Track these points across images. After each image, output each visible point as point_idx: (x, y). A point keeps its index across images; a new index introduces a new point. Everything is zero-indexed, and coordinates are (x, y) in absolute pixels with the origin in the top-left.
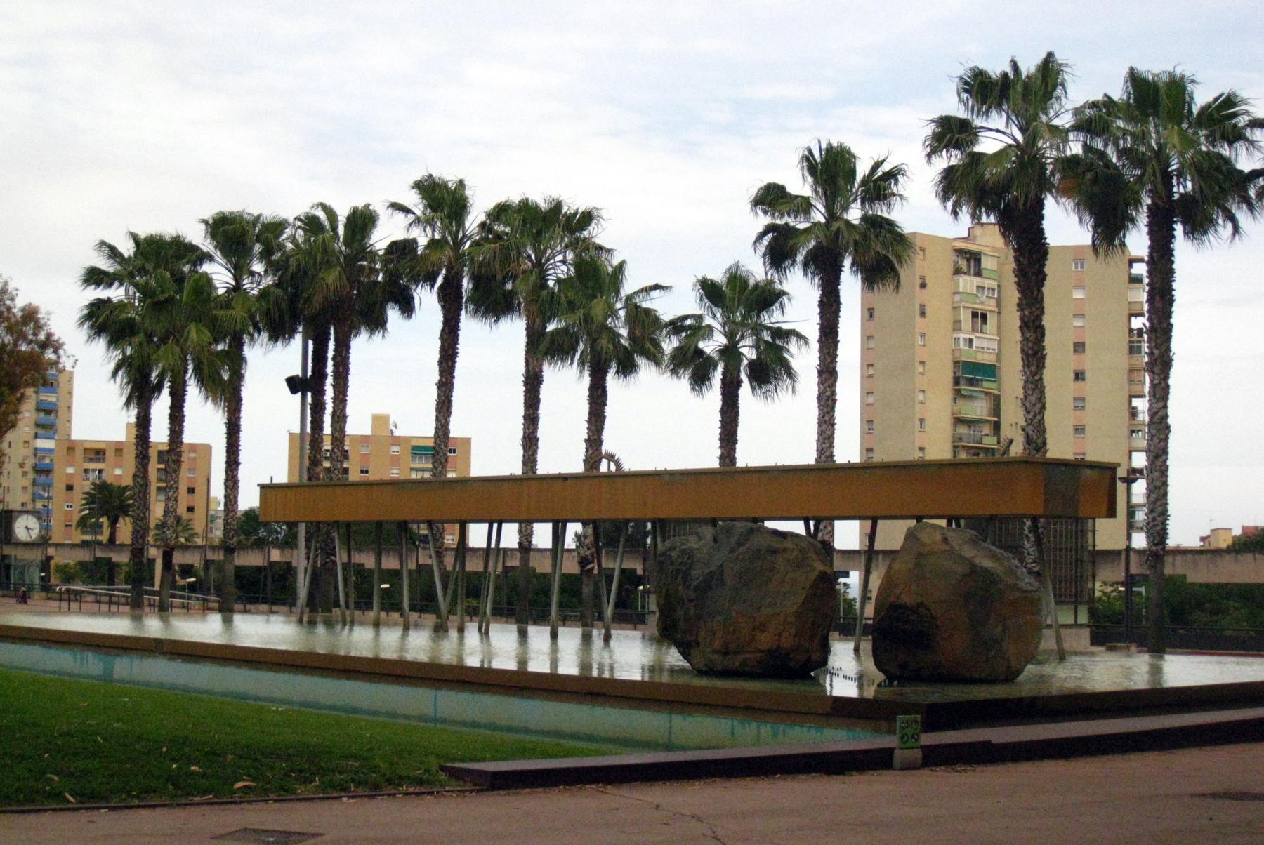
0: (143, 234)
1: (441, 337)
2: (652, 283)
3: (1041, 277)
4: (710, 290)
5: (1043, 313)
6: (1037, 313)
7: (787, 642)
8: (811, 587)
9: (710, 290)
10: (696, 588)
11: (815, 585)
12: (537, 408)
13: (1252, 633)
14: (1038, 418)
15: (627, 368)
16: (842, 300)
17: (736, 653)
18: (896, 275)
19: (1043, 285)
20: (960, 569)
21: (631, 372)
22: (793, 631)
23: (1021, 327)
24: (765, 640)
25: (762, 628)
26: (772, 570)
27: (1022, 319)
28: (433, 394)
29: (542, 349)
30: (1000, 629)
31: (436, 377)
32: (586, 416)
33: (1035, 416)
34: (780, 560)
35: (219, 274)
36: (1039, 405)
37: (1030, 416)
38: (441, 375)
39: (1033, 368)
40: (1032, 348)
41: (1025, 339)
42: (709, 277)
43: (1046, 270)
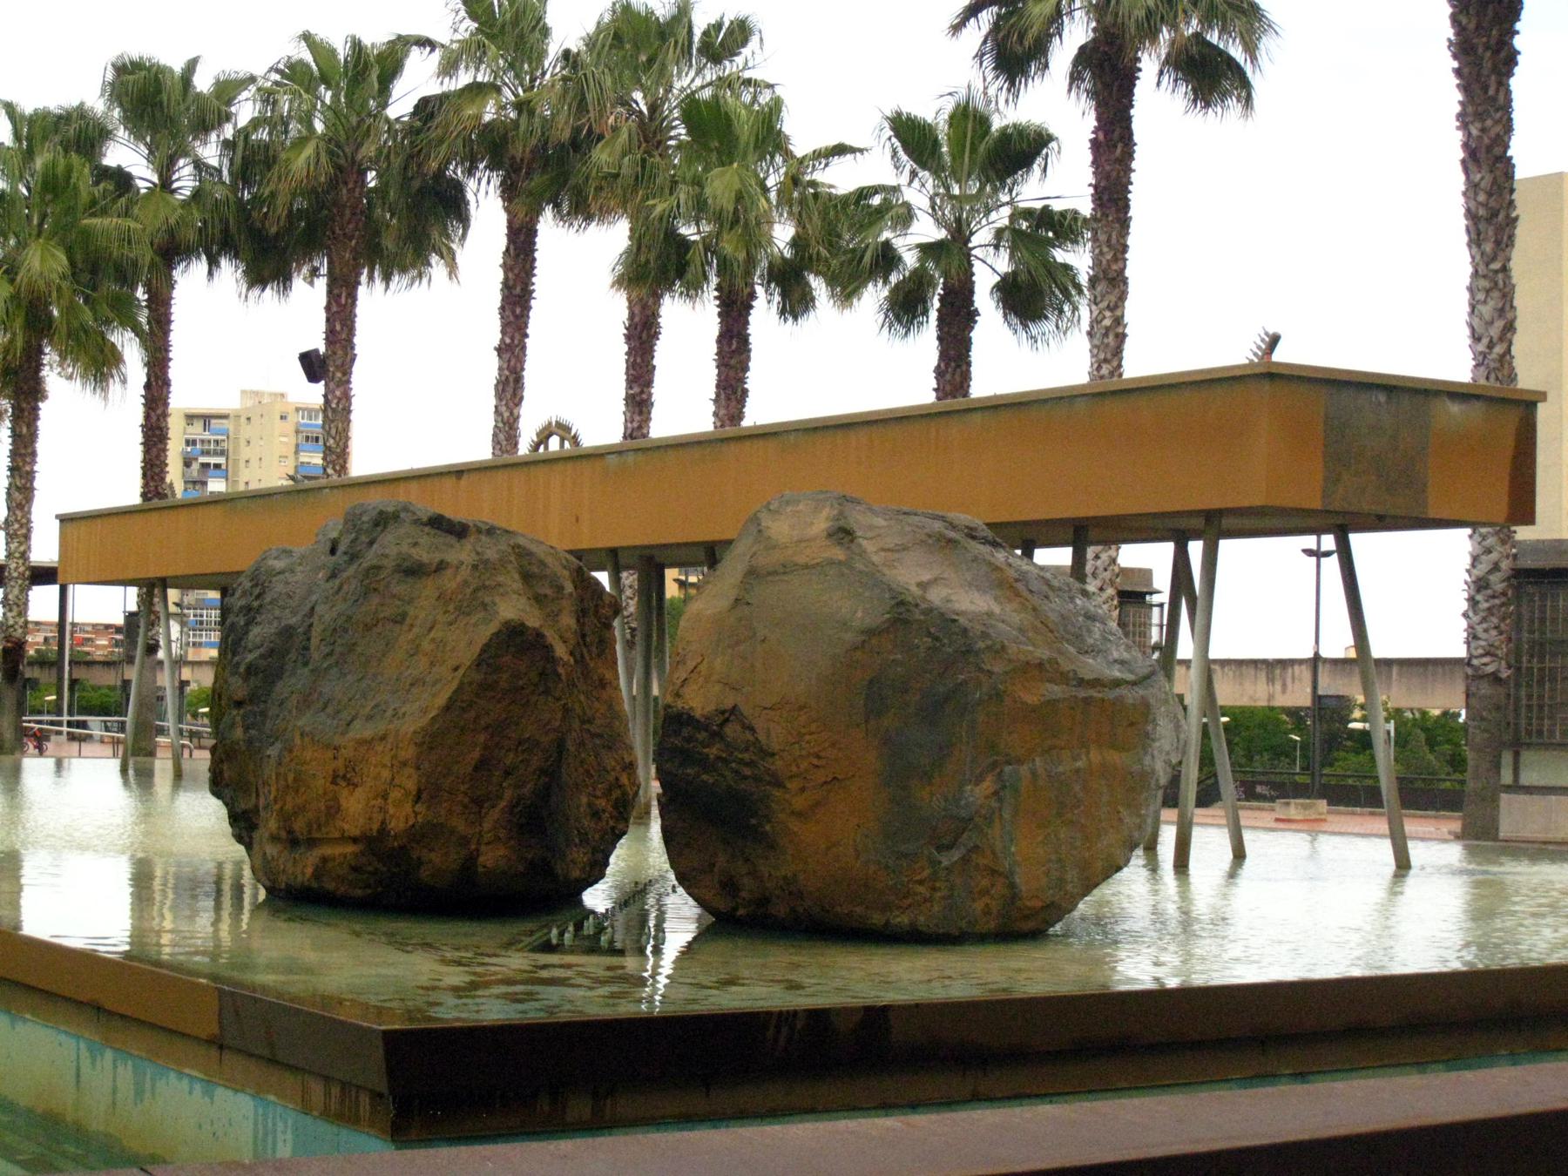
0: (27, 107)
1: (505, 266)
2: (832, 142)
3: (1508, 60)
4: (912, 137)
5: (1509, 129)
6: (1498, 129)
7: (401, 816)
8: (478, 664)
9: (912, 137)
10: (251, 670)
11: (488, 658)
12: (649, 383)
13: (753, 821)
14: (1499, 349)
15: (796, 304)
16: (1136, 138)
17: (312, 843)
18: (1245, 84)
19: (1510, 74)
20: (862, 612)
21: (806, 310)
22: (411, 785)
23: (1463, 162)
24: (356, 808)
25: (345, 777)
26: (400, 619)
27: (1465, 146)
28: (491, 367)
29: (654, 272)
30: (988, 785)
31: (495, 336)
32: (711, 391)
33: (1491, 346)
34: (427, 590)
35: (126, 154)
36: (1500, 324)
37: (1481, 347)
38: (503, 332)
39: (1488, 247)
40: (1485, 205)
41: (1472, 189)
42: (905, 110)
43: (1518, 42)
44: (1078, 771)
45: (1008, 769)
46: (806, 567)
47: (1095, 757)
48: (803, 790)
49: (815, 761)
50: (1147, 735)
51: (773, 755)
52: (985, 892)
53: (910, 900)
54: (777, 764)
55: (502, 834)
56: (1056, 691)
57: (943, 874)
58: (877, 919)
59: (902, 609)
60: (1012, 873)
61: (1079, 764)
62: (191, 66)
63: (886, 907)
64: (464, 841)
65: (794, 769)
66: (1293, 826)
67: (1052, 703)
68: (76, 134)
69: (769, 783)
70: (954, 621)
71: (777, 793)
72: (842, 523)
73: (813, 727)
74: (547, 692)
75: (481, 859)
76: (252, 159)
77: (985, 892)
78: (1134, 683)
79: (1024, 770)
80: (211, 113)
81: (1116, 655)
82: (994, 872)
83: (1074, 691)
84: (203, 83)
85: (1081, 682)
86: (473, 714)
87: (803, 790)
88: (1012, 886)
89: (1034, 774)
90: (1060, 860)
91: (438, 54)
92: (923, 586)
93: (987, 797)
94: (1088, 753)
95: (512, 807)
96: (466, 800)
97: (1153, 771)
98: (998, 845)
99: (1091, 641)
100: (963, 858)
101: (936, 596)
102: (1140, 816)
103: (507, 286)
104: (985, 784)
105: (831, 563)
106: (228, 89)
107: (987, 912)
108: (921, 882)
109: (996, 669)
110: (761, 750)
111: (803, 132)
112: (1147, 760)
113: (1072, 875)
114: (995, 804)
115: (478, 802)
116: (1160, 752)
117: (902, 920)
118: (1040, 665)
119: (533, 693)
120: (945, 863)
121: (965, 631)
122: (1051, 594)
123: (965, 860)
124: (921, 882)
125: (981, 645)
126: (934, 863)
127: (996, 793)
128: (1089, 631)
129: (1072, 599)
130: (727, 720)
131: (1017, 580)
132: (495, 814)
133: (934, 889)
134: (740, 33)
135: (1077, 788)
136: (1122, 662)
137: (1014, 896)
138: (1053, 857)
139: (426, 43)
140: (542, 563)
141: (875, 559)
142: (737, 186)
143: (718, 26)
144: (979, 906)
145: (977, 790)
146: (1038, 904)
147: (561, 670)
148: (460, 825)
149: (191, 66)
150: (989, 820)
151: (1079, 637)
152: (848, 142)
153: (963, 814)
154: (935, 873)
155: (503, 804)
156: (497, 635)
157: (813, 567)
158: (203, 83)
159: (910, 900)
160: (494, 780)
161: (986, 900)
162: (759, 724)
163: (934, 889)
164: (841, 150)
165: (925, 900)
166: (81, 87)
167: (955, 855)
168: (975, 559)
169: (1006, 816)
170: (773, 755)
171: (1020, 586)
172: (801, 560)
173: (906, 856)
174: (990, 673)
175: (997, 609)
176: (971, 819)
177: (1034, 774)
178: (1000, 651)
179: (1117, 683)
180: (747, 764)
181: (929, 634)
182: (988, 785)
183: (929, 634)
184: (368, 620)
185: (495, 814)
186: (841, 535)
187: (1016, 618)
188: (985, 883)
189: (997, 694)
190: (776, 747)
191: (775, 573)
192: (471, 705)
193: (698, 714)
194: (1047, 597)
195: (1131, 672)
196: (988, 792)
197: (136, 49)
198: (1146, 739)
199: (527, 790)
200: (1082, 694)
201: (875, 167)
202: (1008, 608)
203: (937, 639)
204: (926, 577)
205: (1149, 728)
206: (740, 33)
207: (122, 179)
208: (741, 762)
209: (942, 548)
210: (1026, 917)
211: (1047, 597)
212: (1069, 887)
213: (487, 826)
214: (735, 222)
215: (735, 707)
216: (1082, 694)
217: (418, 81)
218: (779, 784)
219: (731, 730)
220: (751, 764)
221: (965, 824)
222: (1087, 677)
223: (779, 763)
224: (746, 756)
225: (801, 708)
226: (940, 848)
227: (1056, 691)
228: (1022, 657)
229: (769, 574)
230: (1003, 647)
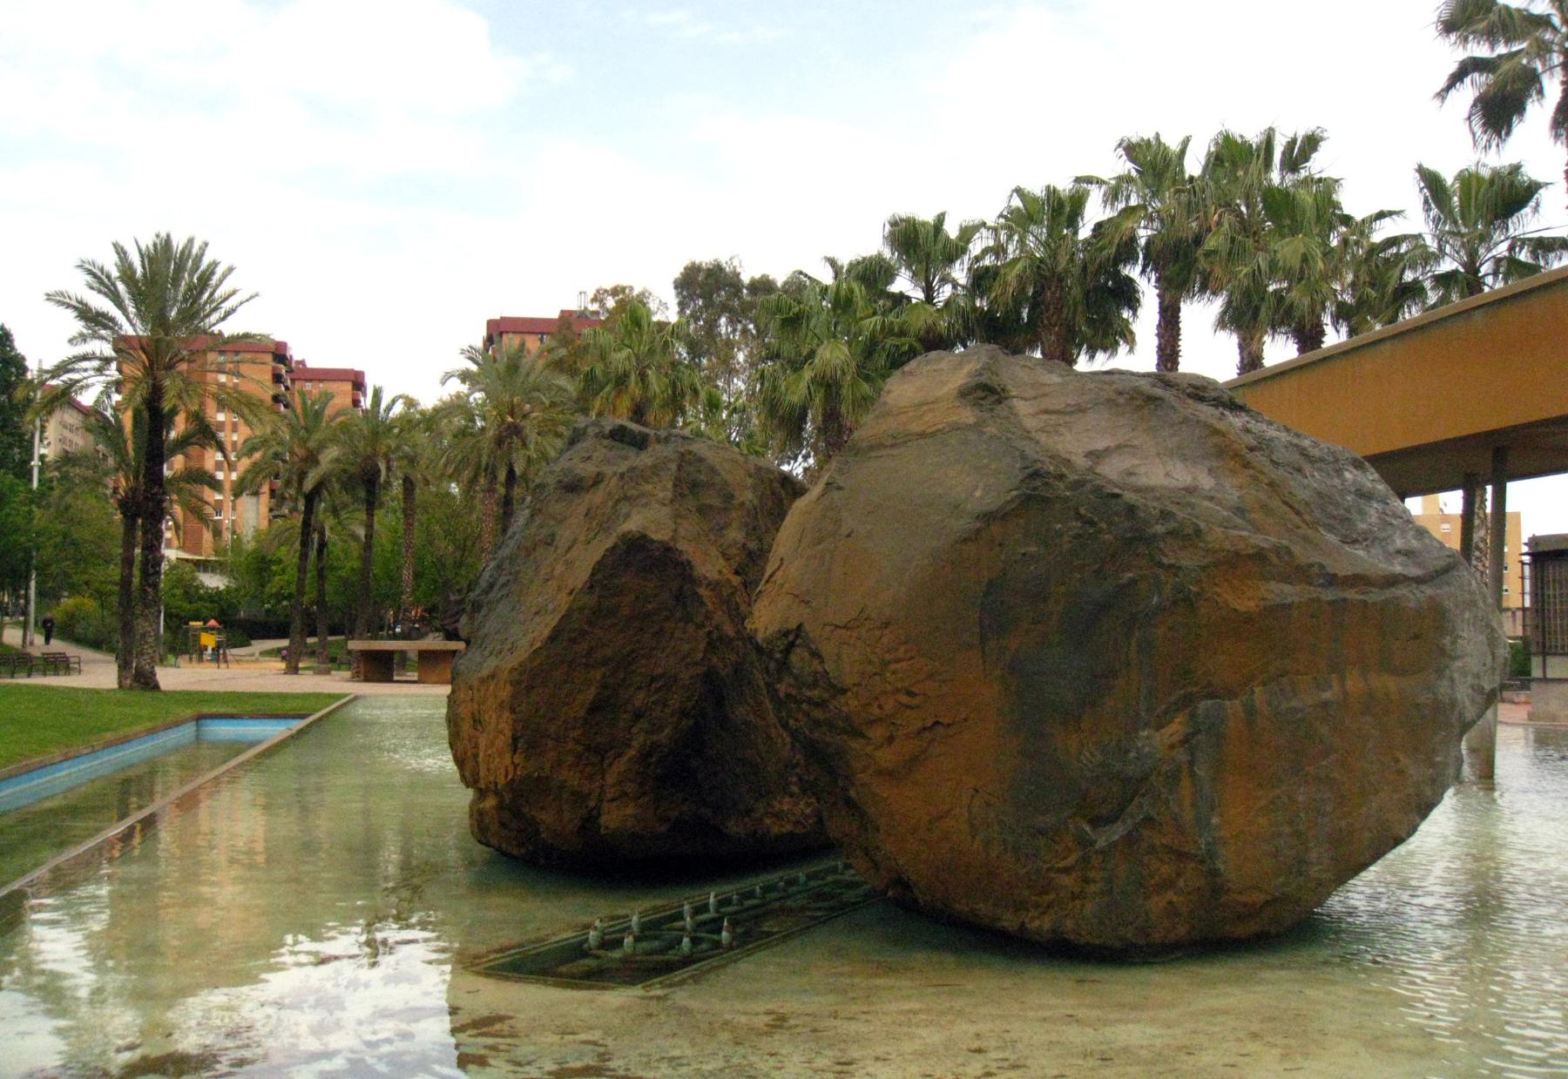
1: (1158, 335)
8: (591, 586)
11: (604, 576)
30: (1177, 728)
44: (1325, 705)
45: (1204, 705)
46: (922, 435)
47: (1354, 683)
48: (891, 739)
49: (904, 699)
50: (1442, 652)
51: (844, 691)
52: (1169, 884)
53: (1052, 896)
54: (850, 704)
55: (631, 788)
56: (1290, 592)
57: (1096, 860)
58: (1008, 921)
59: (1038, 483)
60: (1212, 855)
61: (1327, 695)
62: (941, 219)
63: (1020, 906)
64: (579, 797)
65: (876, 711)
66: (679, 975)
67: (1281, 610)
68: (872, 274)
69: (844, 731)
70: (1117, 496)
71: (856, 744)
72: (984, 379)
73: (901, 653)
74: (687, 619)
75: (603, 819)
76: (981, 279)
77: (1169, 884)
78: (1419, 581)
79: (1233, 707)
80: (954, 252)
81: (1399, 543)
82: (1181, 856)
83: (1313, 592)
84: (952, 230)
85: (1332, 580)
86: (585, 646)
87: (891, 739)
88: (1214, 873)
89: (1251, 711)
90: (1297, 834)
91: (1104, 188)
92: (1093, 455)
93: (1172, 747)
94: (1342, 679)
95: (644, 756)
96: (580, 748)
97: (1453, 703)
98: (1188, 815)
99: (1362, 526)
100: (1129, 834)
101: (1111, 469)
102: (1434, 765)
103: (1161, 349)
104: (1174, 727)
105: (956, 428)
106: (968, 233)
107: (1172, 911)
108: (1066, 870)
109: (1184, 563)
110: (833, 686)
111: (1354, 203)
112: (1443, 687)
113: (1319, 856)
114: (1182, 756)
115: (600, 752)
116: (1464, 674)
117: (1040, 924)
118: (1260, 556)
119: (667, 619)
120: (1101, 843)
121: (1131, 509)
122: (1307, 468)
123: (1130, 839)
124: (1066, 870)
125: (1160, 529)
126: (1084, 843)
127: (1185, 741)
128: (1362, 513)
129: (1339, 472)
130: (792, 645)
131: (1252, 449)
132: (620, 765)
133: (1086, 881)
134: (1312, 143)
135: (1324, 730)
136: (1408, 553)
137: (1216, 887)
138: (1287, 829)
139: (1100, 182)
140: (713, 470)
141: (1030, 423)
142: (1302, 250)
143: (1294, 141)
144: (1157, 904)
145: (1157, 737)
146: (1258, 897)
147: (702, 591)
148: (571, 778)
149: (941, 219)
150: (1173, 778)
151: (1344, 520)
152: (1386, 208)
153: (1130, 770)
154: (1085, 859)
155: (632, 752)
156: (614, 547)
157: (933, 434)
158: (952, 230)
159: (1052, 896)
160: (622, 724)
161: (1170, 895)
162: (828, 649)
163: (1086, 881)
164: (1381, 215)
165: (1074, 897)
166: (871, 243)
167: (1117, 831)
168: (1185, 421)
169: (1201, 772)
170: (844, 691)
171: (1258, 459)
172: (915, 427)
173: (1042, 832)
174: (1174, 569)
175: (1207, 482)
176: (1144, 779)
177: (1251, 711)
178: (1189, 536)
179: (1392, 581)
180: (817, 705)
181: (1079, 517)
182: (1177, 728)
183: (1079, 517)
184: (528, 544)
185: (620, 765)
186: (980, 394)
187: (1233, 496)
188: (1166, 870)
189: (1187, 599)
190: (848, 681)
191: (882, 446)
192: (583, 633)
193: (760, 637)
194: (1299, 470)
195: (1419, 565)
196: (1175, 739)
197: (904, 212)
198: (1444, 655)
199: (664, 736)
200: (1329, 595)
201: (1415, 220)
202: (1228, 483)
203: (1092, 523)
204: (1100, 444)
205: (1447, 641)
206: (1312, 143)
207: (901, 299)
208: (809, 701)
209: (1140, 408)
210: (1240, 918)
211: (1299, 470)
212: (1314, 871)
213: (610, 779)
214: (1300, 279)
215: (800, 627)
216: (1329, 595)
217: (1096, 211)
218: (857, 733)
219: (798, 658)
220: (821, 704)
221: (1134, 786)
222: (1341, 573)
223: (853, 703)
224: (815, 694)
225: (886, 624)
226: (1096, 822)
227: (1290, 592)
228: (1227, 546)
229: (871, 448)
230: (1198, 532)
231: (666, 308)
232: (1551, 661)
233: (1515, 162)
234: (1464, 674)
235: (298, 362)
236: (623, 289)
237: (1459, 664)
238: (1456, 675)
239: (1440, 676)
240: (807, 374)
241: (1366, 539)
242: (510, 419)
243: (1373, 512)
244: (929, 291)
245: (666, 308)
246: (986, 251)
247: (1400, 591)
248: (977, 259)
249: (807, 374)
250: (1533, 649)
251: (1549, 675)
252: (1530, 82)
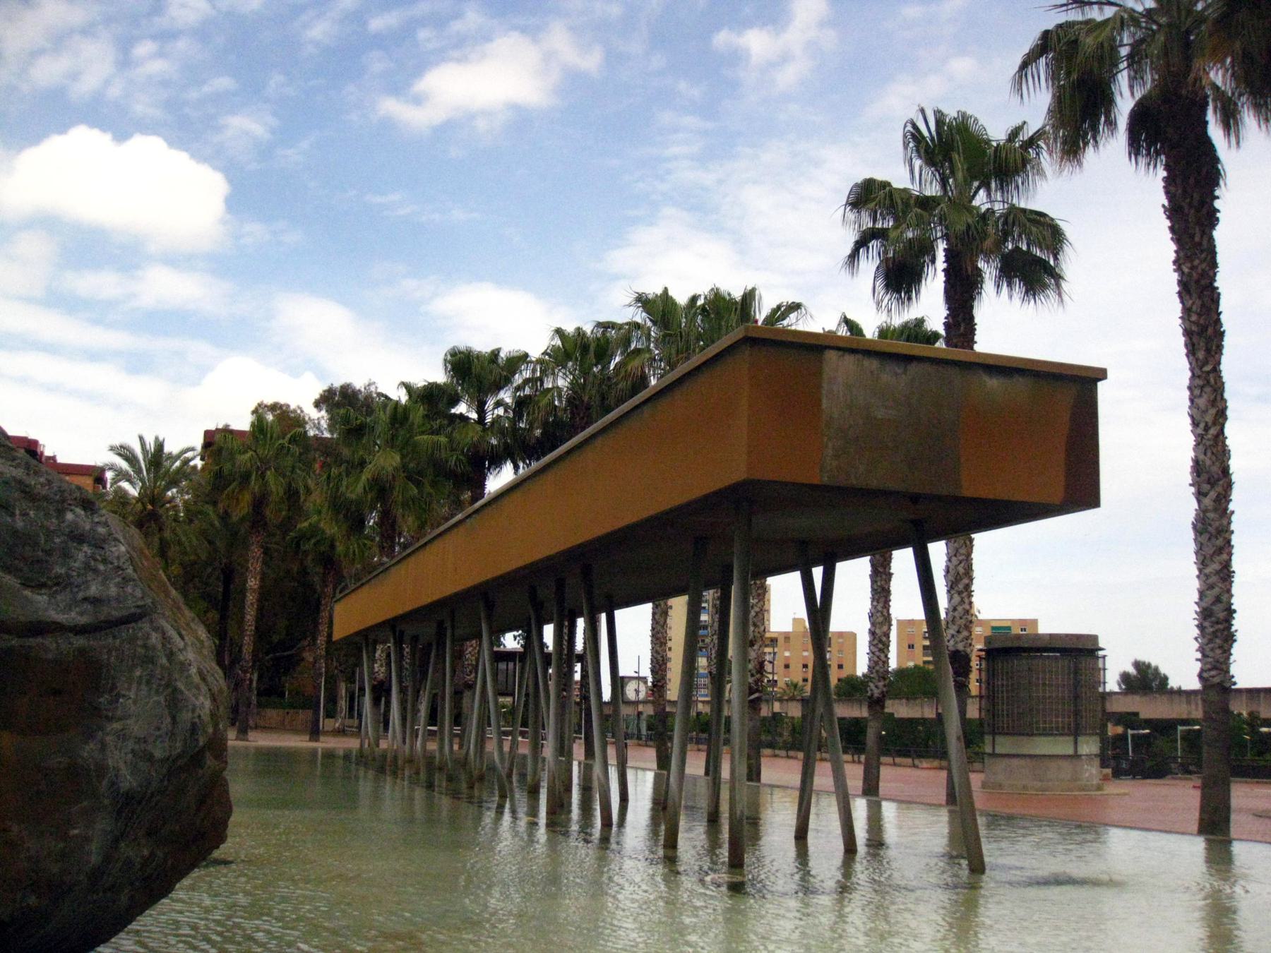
68: (430, 397)
97: (101, 770)
99: (59, 570)
128: (66, 555)
129: (61, 513)
207: (462, 417)
231: (317, 420)
232: (999, 739)
233: (919, 316)
234: (122, 736)
235: (49, 458)
236: (281, 406)
237: (117, 726)
238: (108, 739)
239: (90, 736)
240: (366, 476)
241: (61, 583)
242: (150, 507)
243: (81, 556)
244: (481, 412)
245: (317, 420)
246: (526, 381)
247: (49, 642)
248: (518, 388)
249: (366, 476)
250: (986, 729)
251: (998, 751)
252: (926, 249)
